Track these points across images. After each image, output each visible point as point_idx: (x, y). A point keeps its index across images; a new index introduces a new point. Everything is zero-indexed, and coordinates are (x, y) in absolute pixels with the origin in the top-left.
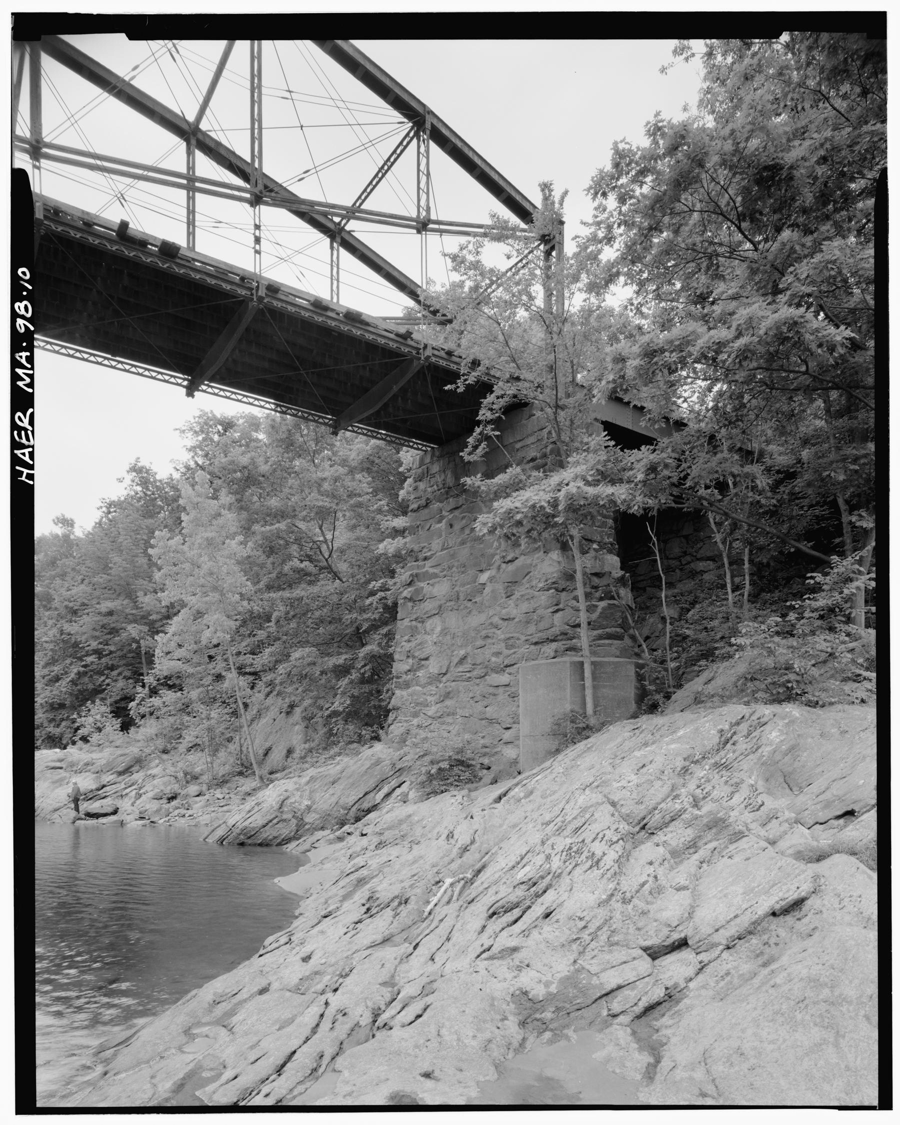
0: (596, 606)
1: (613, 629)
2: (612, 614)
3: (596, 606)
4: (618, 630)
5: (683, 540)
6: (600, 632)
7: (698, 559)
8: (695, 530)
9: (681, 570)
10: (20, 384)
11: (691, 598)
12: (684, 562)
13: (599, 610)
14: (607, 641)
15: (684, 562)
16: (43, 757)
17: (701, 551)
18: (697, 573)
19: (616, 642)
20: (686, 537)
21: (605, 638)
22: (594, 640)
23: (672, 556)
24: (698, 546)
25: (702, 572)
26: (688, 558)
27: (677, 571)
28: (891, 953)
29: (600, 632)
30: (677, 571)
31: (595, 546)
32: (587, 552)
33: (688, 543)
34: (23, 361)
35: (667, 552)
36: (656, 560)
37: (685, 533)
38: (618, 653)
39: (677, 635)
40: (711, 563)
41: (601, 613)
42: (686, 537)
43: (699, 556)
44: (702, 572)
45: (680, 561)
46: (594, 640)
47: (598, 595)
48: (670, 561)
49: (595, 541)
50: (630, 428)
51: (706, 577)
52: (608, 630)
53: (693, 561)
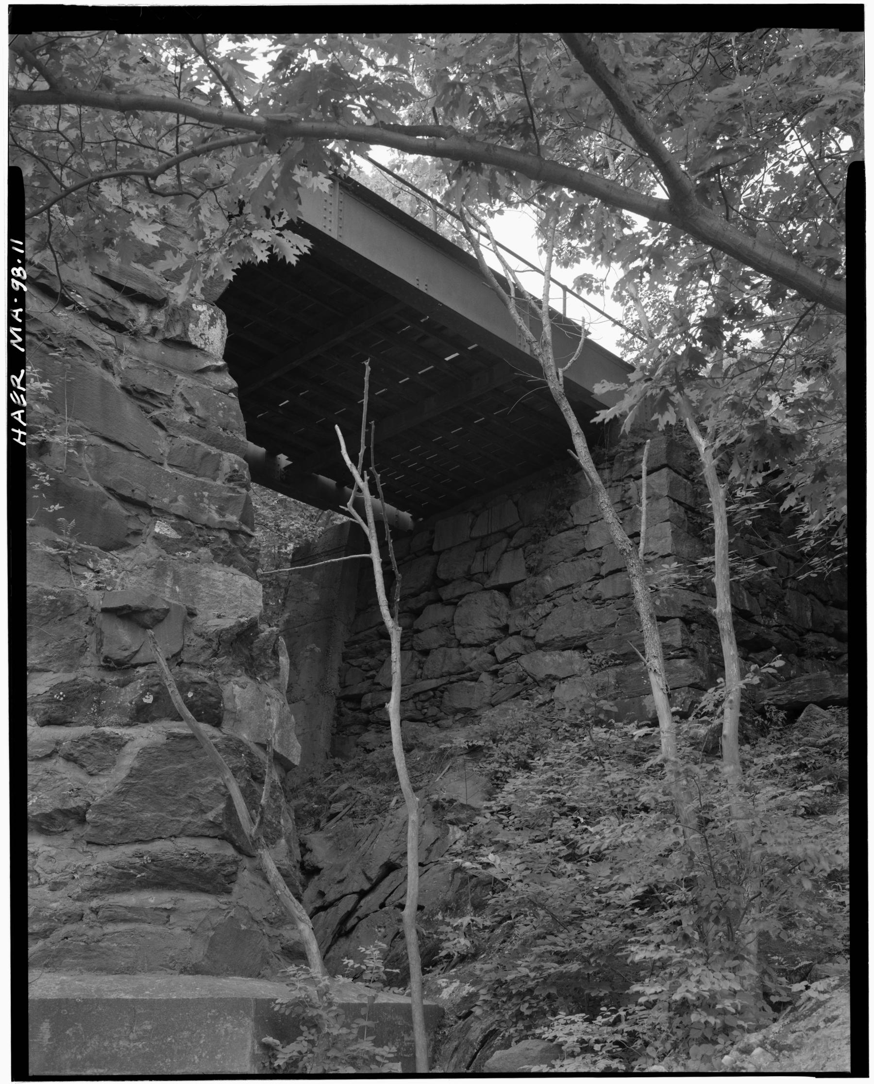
0: (118, 744)
1: (186, 844)
2: (183, 777)
3: (118, 744)
4: (206, 846)
5: (498, 596)
6: (123, 853)
7: (539, 647)
8: (530, 570)
9: (495, 673)
10: (12, 341)
11: (519, 748)
12: (501, 655)
13: (128, 761)
14: (152, 899)
15: (501, 655)
16: (843, 861)
17: (548, 625)
18: (537, 683)
19: (192, 900)
20: (506, 589)
21: (145, 885)
22: (94, 892)
23: (470, 639)
24: (540, 610)
25: (550, 681)
26: (514, 644)
27: (484, 677)
28: (95, 8)
29: (123, 853)
30: (484, 677)
31: (161, 528)
32: (122, 546)
33: (511, 604)
34: (19, 419)
35: (458, 630)
36: (370, 562)
37: (503, 578)
38: (198, 953)
39: (225, 787)
40: (576, 655)
41: (134, 773)
42: (506, 589)
43: (541, 638)
44: (550, 681)
45: (492, 653)
46: (94, 892)
47: (128, 696)
48: (466, 651)
49: (162, 513)
50: (334, 235)
51: (563, 692)
52: (156, 847)
53: (527, 650)
